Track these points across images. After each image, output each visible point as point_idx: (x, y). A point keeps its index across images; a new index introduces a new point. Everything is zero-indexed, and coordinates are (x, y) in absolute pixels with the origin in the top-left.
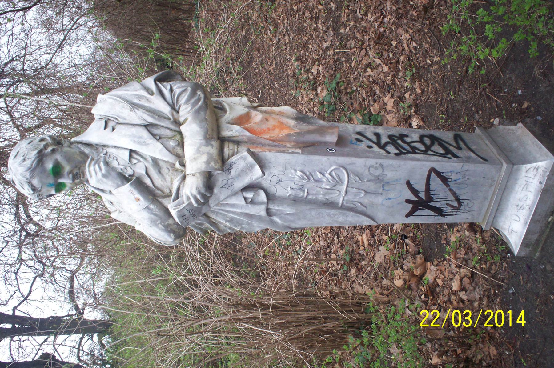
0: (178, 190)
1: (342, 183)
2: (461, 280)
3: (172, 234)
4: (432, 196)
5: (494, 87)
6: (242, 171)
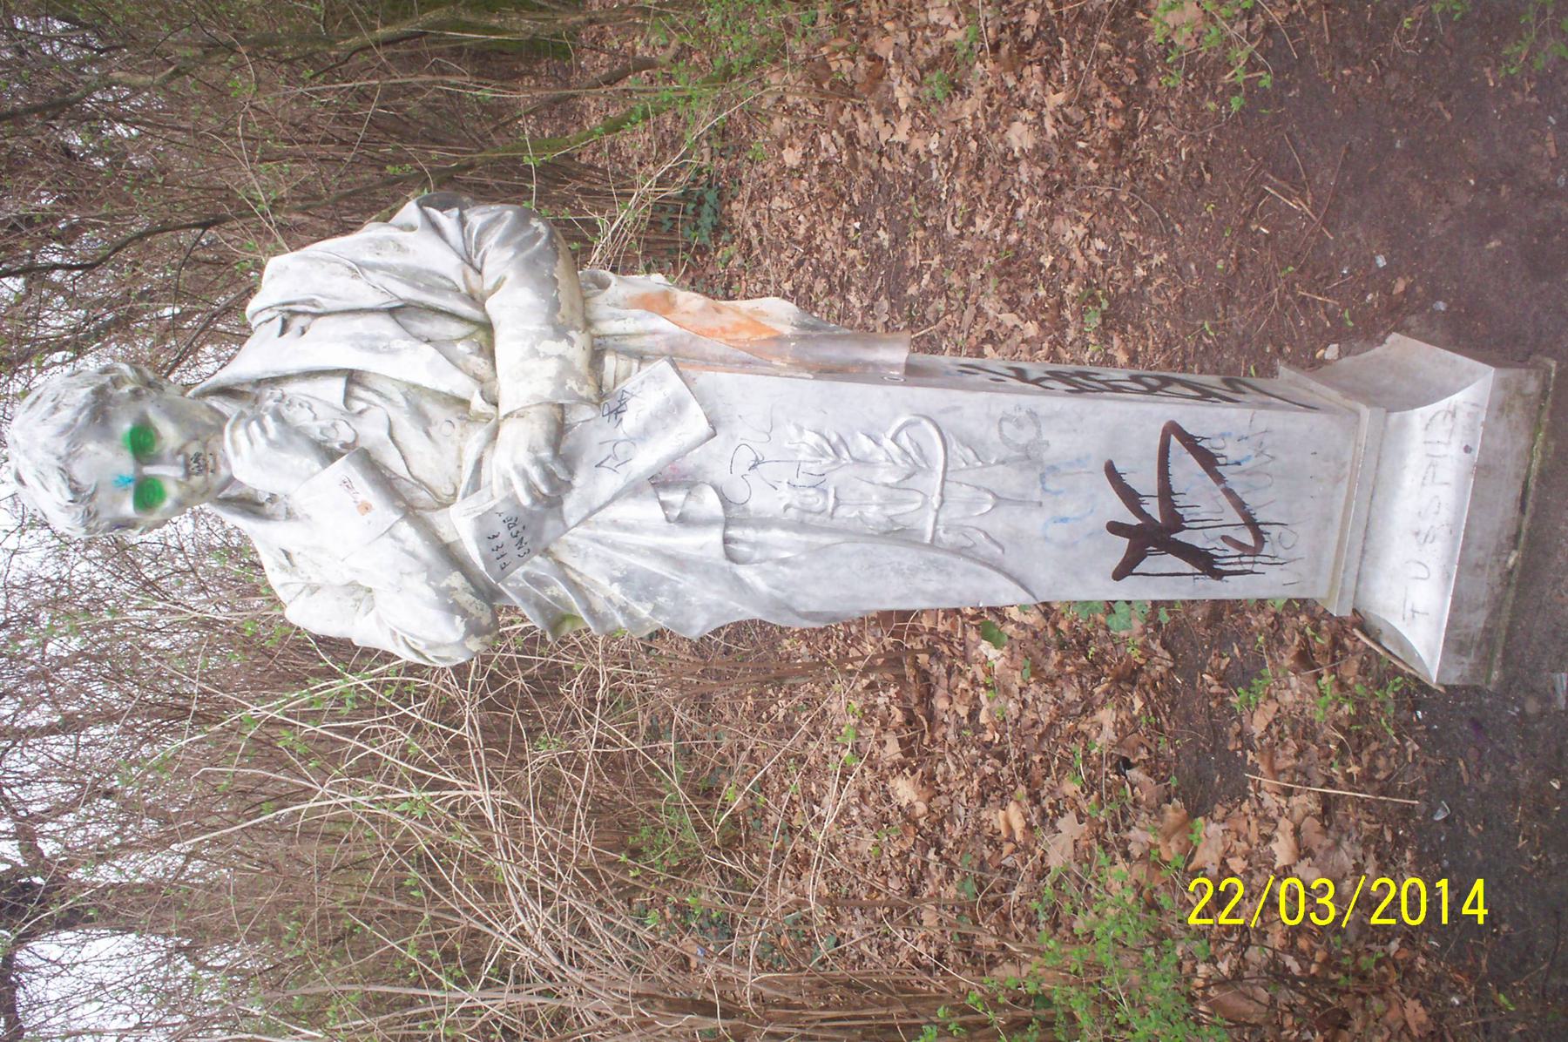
0: (479, 463)
1: (930, 469)
2: (1297, 831)
3: (458, 618)
4: (1180, 511)
5: (1315, 272)
6: (655, 417)
